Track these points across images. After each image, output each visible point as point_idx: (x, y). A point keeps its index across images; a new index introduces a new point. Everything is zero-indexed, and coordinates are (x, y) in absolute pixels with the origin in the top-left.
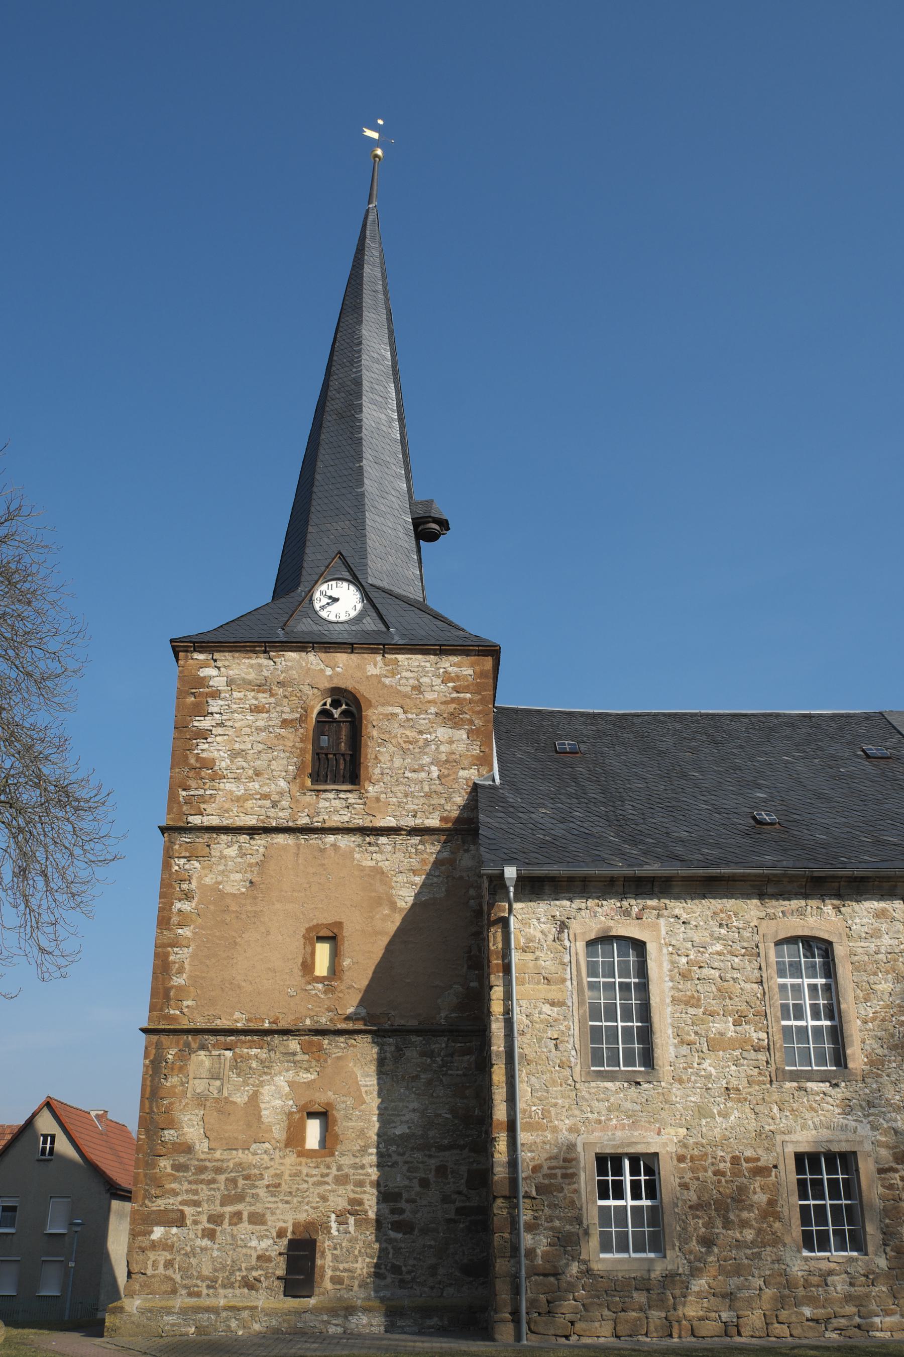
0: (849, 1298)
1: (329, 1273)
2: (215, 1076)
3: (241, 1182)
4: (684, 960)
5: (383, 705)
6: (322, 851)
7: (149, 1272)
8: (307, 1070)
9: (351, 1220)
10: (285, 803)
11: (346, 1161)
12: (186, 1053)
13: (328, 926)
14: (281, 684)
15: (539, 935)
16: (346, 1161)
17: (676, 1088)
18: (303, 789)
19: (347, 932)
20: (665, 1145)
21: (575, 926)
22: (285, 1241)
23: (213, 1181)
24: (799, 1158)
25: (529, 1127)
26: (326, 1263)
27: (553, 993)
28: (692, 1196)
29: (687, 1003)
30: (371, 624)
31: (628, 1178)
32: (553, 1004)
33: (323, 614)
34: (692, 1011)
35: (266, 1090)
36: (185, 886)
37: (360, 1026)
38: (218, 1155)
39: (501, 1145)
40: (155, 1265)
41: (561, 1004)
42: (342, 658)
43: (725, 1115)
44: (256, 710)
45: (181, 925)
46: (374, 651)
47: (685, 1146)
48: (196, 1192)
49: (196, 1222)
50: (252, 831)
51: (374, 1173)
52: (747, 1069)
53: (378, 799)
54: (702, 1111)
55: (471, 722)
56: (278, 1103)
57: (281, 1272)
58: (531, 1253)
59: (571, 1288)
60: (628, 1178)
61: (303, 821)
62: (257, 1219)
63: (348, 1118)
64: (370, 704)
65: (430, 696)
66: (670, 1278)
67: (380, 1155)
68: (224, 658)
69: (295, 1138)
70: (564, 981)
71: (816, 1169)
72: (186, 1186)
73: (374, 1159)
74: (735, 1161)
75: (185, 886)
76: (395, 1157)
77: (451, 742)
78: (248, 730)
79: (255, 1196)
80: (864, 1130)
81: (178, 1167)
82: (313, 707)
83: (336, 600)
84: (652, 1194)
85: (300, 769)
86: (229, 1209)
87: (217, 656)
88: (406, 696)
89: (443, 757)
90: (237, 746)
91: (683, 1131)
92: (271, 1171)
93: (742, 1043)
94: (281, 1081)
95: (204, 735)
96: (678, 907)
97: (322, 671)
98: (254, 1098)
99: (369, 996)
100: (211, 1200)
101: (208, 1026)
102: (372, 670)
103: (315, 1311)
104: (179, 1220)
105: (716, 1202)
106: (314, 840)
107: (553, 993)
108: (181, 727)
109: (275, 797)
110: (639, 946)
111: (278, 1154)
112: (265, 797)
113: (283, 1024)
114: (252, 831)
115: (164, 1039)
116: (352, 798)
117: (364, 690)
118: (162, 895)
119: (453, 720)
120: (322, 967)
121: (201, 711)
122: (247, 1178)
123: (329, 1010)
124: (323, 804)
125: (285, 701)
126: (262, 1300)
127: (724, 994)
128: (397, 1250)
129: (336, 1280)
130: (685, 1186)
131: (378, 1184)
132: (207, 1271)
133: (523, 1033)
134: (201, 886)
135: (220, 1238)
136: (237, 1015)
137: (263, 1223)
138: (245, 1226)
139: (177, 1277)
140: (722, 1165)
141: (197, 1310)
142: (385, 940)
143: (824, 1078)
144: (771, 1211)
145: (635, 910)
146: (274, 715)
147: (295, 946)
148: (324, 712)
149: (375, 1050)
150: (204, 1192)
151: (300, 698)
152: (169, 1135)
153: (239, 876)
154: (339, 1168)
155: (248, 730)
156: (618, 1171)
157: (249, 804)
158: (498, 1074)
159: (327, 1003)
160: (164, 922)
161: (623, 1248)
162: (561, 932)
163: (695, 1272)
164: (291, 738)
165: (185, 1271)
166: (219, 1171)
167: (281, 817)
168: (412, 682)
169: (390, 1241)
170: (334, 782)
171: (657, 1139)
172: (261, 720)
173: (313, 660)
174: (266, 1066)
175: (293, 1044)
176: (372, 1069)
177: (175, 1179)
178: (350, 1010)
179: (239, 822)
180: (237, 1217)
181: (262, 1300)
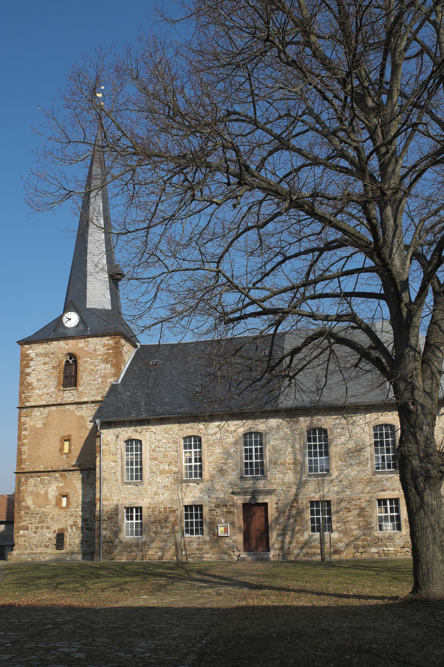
0: (197, 549)
1: (68, 543)
2: (35, 486)
3: (43, 517)
4: (154, 446)
5: (84, 358)
6: (65, 411)
7: (20, 543)
8: (61, 483)
9: (74, 527)
10: (54, 396)
11: (72, 510)
12: (26, 480)
13: (67, 436)
14: (52, 354)
15: (110, 440)
16: (72, 510)
17: (149, 486)
18: (59, 390)
19: (73, 438)
20: (144, 504)
21: (121, 436)
22: (56, 534)
23: (36, 517)
24: (186, 507)
25: (106, 500)
26: (67, 540)
27: (114, 458)
28: (152, 520)
29: (154, 459)
30: (82, 327)
31: (134, 514)
32: (114, 462)
33: (66, 325)
34: (155, 462)
35: (50, 489)
36: (25, 426)
37: (77, 468)
38: (37, 509)
39: (98, 506)
40: (21, 541)
41: (116, 462)
42: (71, 342)
43: (163, 494)
44: (45, 364)
45: (24, 439)
46: (81, 338)
47: (150, 504)
48: (31, 520)
49: (31, 529)
50: (44, 406)
51: (80, 513)
52: (171, 480)
53: (82, 392)
54: (156, 494)
55: (112, 361)
56: (53, 493)
57: (55, 543)
58: (105, 536)
59: (116, 547)
60: (134, 514)
61: (59, 401)
62: (48, 528)
63: (73, 497)
64: (80, 358)
65: (99, 353)
66: (145, 543)
67: (82, 508)
68: (34, 346)
69: (58, 503)
70: (117, 454)
71: (191, 510)
72: (28, 519)
73: (81, 509)
74: (165, 508)
75: (25, 426)
76: (86, 508)
77: (105, 369)
78: (42, 371)
79: (47, 521)
80: (206, 498)
81: (26, 513)
82: (62, 361)
83: (70, 319)
84: (141, 519)
85: (59, 383)
86: (40, 525)
87: (32, 345)
88: (91, 354)
89: (103, 375)
90: (39, 377)
91: (150, 500)
92: (52, 514)
93: (170, 472)
94: (54, 486)
95: (28, 374)
96: (153, 428)
97: (65, 347)
98: (46, 491)
99: (79, 459)
100: (35, 523)
101: (33, 470)
102: (81, 345)
103: (63, 554)
104: (27, 529)
105: (159, 521)
106: (63, 408)
107: (114, 458)
108: (22, 372)
109: (51, 394)
110: (141, 441)
111: (53, 508)
112: (48, 394)
113: (54, 469)
114: (44, 406)
115: (21, 475)
116: (74, 392)
117: (78, 353)
118: (19, 430)
119: (106, 361)
120: (66, 450)
121: (28, 366)
122: (45, 516)
123: (68, 463)
124: (65, 395)
125: (53, 360)
126: (50, 551)
127: (165, 456)
128: (87, 536)
129: (70, 545)
130: (150, 516)
131: (82, 517)
132: (35, 543)
133: (105, 471)
134: (29, 426)
135: (38, 533)
136: (41, 466)
137: (50, 529)
138: (45, 530)
139: (27, 545)
140: (161, 510)
141: (31, 554)
142: (84, 440)
143: (195, 482)
144: (174, 524)
145: (140, 430)
146: (50, 365)
147: (57, 444)
148: (67, 361)
149: (81, 475)
150: (33, 520)
151: (58, 358)
152: (23, 504)
153: (40, 422)
154: (71, 512)
155: (42, 371)
156: (132, 512)
157: (43, 397)
158: (98, 484)
159: (67, 461)
160: (19, 438)
161: (132, 534)
162: (117, 439)
163: (152, 542)
164: (55, 373)
165: (29, 543)
166: (37, 514)
167: (52, 401)
168: (93, 348)
169: (85, 533)
170: (70, 387)
171: (142, 502)
172: (46, 367)
173: (62, 343)
174: (49, 482)
175: (57, 475)
176: (80, 481)
177: (26, 517)
178: (74, 463)
179: (40, 404)
180: (43, 527)
181: (50, 551)
